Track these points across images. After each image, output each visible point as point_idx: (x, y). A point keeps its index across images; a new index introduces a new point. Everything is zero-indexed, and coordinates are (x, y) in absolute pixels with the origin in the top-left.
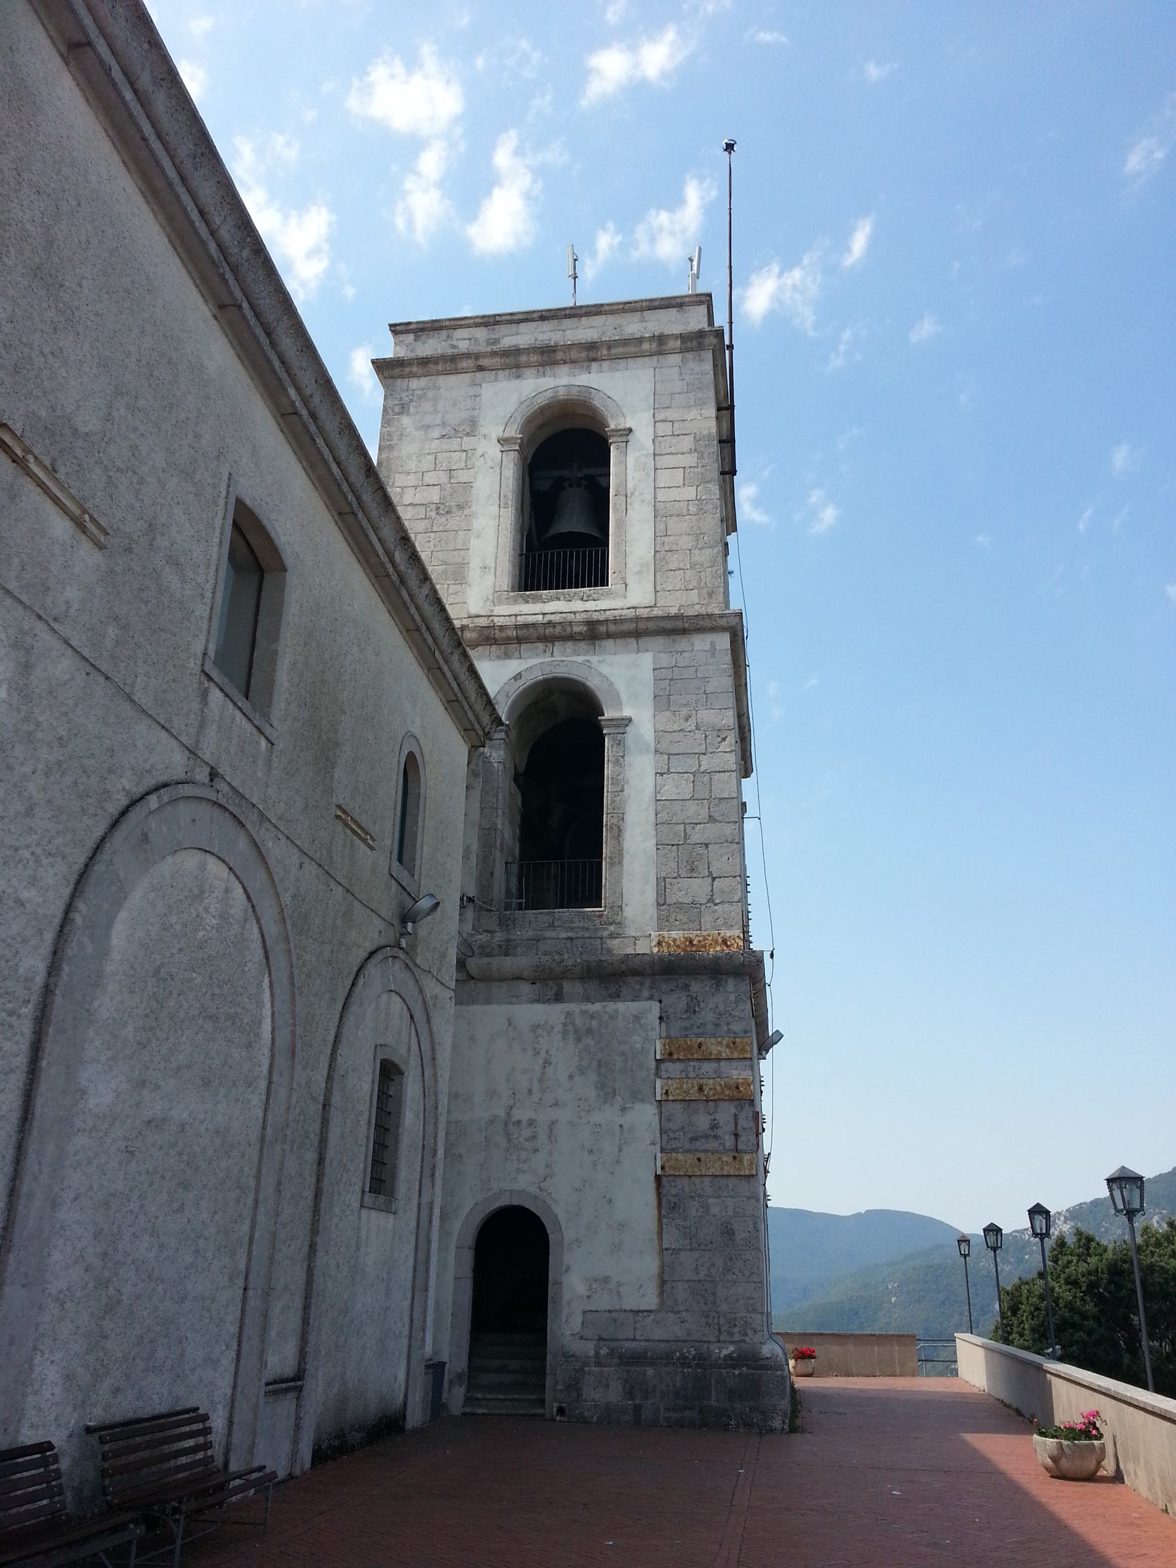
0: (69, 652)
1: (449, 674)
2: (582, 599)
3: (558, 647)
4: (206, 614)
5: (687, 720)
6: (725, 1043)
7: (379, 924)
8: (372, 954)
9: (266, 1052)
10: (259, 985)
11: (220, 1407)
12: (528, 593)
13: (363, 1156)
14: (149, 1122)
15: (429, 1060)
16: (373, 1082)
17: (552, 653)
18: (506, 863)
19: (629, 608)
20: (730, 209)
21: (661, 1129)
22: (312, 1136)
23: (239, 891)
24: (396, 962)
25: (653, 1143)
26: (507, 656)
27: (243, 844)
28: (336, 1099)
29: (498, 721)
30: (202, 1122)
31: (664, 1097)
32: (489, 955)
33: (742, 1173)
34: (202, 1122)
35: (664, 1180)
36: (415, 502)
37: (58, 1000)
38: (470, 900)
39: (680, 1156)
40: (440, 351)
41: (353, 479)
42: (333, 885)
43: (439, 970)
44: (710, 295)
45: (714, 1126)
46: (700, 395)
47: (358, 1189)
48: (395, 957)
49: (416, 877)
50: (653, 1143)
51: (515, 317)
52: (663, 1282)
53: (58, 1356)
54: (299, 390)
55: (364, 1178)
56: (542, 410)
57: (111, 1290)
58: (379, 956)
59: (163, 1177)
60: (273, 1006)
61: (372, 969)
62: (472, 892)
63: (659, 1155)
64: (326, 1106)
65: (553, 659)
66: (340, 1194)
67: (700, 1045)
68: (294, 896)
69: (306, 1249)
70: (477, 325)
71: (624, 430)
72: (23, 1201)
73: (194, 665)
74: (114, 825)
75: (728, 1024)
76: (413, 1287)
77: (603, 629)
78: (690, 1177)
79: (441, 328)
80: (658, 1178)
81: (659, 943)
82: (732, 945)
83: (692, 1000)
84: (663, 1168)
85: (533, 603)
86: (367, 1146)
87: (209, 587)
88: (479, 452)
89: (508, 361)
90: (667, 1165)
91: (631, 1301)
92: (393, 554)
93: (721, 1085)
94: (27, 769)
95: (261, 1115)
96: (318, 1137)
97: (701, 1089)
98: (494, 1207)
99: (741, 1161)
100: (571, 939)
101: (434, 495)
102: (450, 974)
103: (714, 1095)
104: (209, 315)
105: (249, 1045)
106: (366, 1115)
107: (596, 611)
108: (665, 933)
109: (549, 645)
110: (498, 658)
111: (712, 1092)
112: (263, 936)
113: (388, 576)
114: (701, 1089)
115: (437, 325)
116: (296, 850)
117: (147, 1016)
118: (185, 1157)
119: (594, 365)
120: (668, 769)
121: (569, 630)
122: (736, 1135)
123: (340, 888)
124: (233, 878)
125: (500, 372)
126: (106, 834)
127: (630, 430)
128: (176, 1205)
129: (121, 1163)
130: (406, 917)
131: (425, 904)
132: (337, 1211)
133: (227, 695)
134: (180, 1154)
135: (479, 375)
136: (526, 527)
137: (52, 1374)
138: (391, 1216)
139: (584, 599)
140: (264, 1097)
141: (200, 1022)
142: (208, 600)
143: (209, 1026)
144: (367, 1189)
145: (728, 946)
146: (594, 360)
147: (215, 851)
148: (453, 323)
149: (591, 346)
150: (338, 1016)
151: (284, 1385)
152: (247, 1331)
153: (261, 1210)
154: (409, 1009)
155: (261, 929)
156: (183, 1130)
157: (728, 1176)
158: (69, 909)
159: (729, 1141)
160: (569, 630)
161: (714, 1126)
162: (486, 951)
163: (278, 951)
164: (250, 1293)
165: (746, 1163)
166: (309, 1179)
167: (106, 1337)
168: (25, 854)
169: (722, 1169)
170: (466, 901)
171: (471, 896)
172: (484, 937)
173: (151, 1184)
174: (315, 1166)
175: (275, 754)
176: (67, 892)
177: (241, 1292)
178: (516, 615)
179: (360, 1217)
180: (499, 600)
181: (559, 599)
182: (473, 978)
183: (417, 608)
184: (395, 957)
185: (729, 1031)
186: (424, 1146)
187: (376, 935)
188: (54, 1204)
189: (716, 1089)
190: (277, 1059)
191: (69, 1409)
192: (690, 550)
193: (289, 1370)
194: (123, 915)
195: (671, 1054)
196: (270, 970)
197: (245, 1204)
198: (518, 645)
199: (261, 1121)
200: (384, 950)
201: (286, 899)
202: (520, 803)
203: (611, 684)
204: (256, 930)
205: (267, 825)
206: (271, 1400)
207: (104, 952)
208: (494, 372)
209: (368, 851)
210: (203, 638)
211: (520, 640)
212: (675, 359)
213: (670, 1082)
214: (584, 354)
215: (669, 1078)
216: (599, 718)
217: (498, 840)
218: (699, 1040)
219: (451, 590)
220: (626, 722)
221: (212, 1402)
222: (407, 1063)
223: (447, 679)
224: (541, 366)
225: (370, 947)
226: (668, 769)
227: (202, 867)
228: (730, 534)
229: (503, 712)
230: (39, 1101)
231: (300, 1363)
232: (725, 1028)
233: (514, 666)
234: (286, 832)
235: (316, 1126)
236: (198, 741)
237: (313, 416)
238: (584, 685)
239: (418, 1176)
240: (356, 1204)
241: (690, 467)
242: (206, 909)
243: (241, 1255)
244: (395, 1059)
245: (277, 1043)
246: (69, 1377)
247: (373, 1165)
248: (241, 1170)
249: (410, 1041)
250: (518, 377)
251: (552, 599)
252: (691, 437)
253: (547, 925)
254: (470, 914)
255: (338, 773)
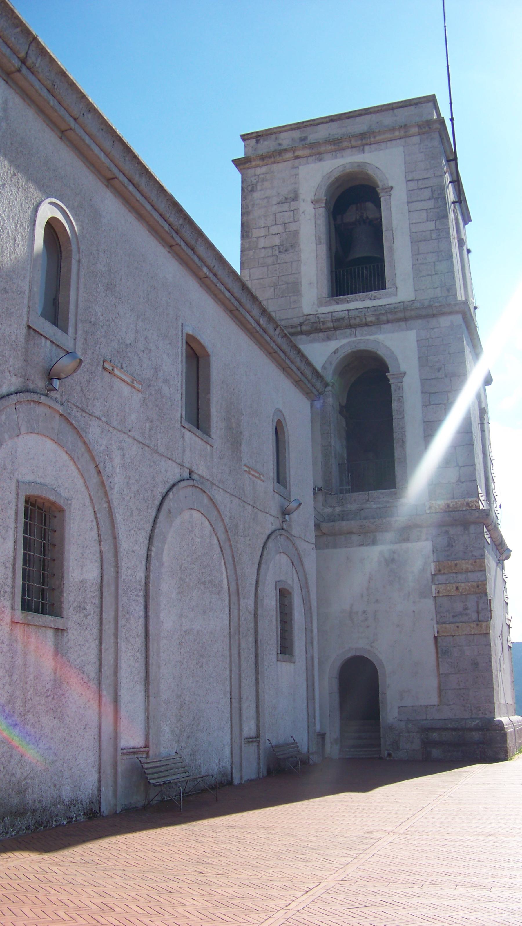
0: (136, 442)
1: (295, 369)
2: (371, 299)
3: (359, 330)
4: (180, 398)
5: (439, 371)
6: (470, 562)
7: (271, 519)
8: (269, 537)
9: (227, 595)
10: (220, 564)
11: (226, 746)
12: (338, 297)
13: (275, 637)
14: (186, 631)
15: (305, 585)
16: (277, 600)
17: (355, 335)
18: (339, 464)
19: (400, 303)
20: (445, 26)
21: (436, 611)
22: (251, 630)
23: (207, 523)
24: (282, 537)
25: (432, 620)
26: (329, 339)
27: (206, 500)
28: (259, 612)
29: (326, 385)
30: (205, 629)
31: (437, 595)
32: (333, 521)
33: (482, 632)
34: (205, 629)
35: (439, 639)
36: (266, 246)
37: (151, 588)
38: (320, 489)
39: (447, 626)
40: (272, 149)
41: (236, 295)
42: (247, 506)
43: (305, 535)
44: (434, 96)
45: (466, 609)
46: (432, 162)
47: (275, 653)
48: (281, 535)
49: (288, 488)
50: (432, 620)
51: (315, 122)
52: (441, 691)
53: (168, 723)
54: (208, 267)
55: (277, 647)
56: (337, 180)
57: (182, 699)
58: (273, 537)
59: (194, 653)
60: (227, 572)
61: (270, 544)
62: (320, 484)
63: (436, 626)
64: (256, 615)
65: (356, 338)
66: (266, 655)
67: (456, 565)
68: (230, 518)
69: (254, 681)
70: (292, 129)
71: (388, 188)
72: (150, 667)
73: (178, 425)
74: (159, 510)
75: (472, 551)
76: (307, 698)
77: (384, 318)
78: (453, 636)
79: (271, 134)
80: (435, 638)
81: (430, 508)
82: (472, 506)
83: (450, 539)
84: (438, 632)
85: (341, 304)
86: (277, 631)
87: (179, 385)
88: (301, 210)
89: (313, 151)
90: (440, 631)
91: (423, 702)
92: (259, 322)
93: (468, 586)
94: (128, 498)
95: (228, 623)
96: (253, 630)
97: (457, 588)
98: (347, 657)
99: (481, 626)
100: (380, 508)
101: (276, 241)
102: (311, 535)
103: (465, 592)
104: (166, 253)
105: (219, 593)
106: (275, 617)
107: (380, 306)
108: (434, 502)
109: (353, 330)
110: (324, 340)
111: (464, 590)
112: (219, 541)
113: (257, 332)
114: (457, 588)
115: (269, 132)
116: (228, 494)
117: (179, 587)
118: (201, 645)
119: (367, 148)
120: (430, 402)
121: (364, 320)
122: (478, 613)
123: (250, 507)
124: (203, 518)
125: (309, 158)
126: (156, 514)
127: (392, 188)
128: (200, 665)
129: (178, 649)
130: (285, 512)
131: (293, 505)
132: (266, 663)
133: (192, 432)
134: (198, 643)
135: (297, 161)
136: (334, 251)
137: (167, 729)
138: (292, 665)
139: (372, 298)
140: (228, 615)
141: (199, 586)
142: (180, 391)
143: (202, 587)
144: (279, 652)
145: (470, 507)
146: (367, 144)
147: (195, 508)
148: (279, 130)
149: (362, 136)
150: (256, 571)
151: (251, 740)
152: (233, 715)
153: (233, 664)
154: (291, 560)
155: (218, 538)
156: (198, 633)
157: (474, 634)
158: (149, 550)
159: (474, 616)
160: (364, 320)
161: (466, 609)
162: (331, 519)
163: (226, 546)
164: (233, 700)
165: (484, 628)
166: (251, 649)
167: (182, 717)
168: (132, 532)
169: (471, 631)
170: (317, 490)
171: (319, 486)
172: (329, 510)
173: (190, 657)
174: (254, 644)
175: (214, 450)
176: (147, 542)
177: (229, 700)
178: (332, 312)
179: (277, 665)
180: (321, 304)
181: (357, 300)
182: (325, 534)
183: (274, 342)
184: (281, 535)
185: (472, 555)
186: (306, 628)
187: (270, 526)
188: (159, 667)
189: (466, 589)
190: (231, 596)
191: (174, 742)
192: (434, 262)
193: (253, 733)
194: (166, 546)
195: (440, 571)
196: (223, 556)
197: (226, 662)
198: (334, 332)
199: (228, 625)
200: (275, 533)
201: (227, 520)
202: (344, 426)
203: (392, 353)
204: (215, 537)
205: (215, 487)
206: (247, 745)
207: (162, 564)
208: (305, 159)
209: (262, 483)
210: (180, 410)
211: (335, 329)
212: (416, 139)
213: (440, 586)
214: (359, 142)
215: (439, 584)
216: (387, 374)
217: (333, 452)
218: (456, 562)
219: (292, 300)
220: (402, 375)
221: (223, 745)
222: (292, 588)
223: (294, 372)
224: (334, 151)
225: (268, 532)
226: (430, 402)
227: (191, 516)
228: (467, 224)
229: (329, 377)
230: (151, 628)
231: (257, 731)
232: (470, 554)
233: (333, 345)
234: (223, 487)
235: (252, 625)
236: (183, 460)
237: (215, 275)
238: (376, 353)
239: (304, 644)
240: (274, 660)
241: (431, 209)
242: (195, 535)
243: (228, 683)
244: (286, 587)
245: (231, 589)
246: (173, 731)
247: (281, 640)
248: (223, 648)
249: (293, 576)
250: (320, 160)
251: (352, 301)
252: (429, 190)
253: (364, 501)
254: (320, 498)
255: (244, 448)
